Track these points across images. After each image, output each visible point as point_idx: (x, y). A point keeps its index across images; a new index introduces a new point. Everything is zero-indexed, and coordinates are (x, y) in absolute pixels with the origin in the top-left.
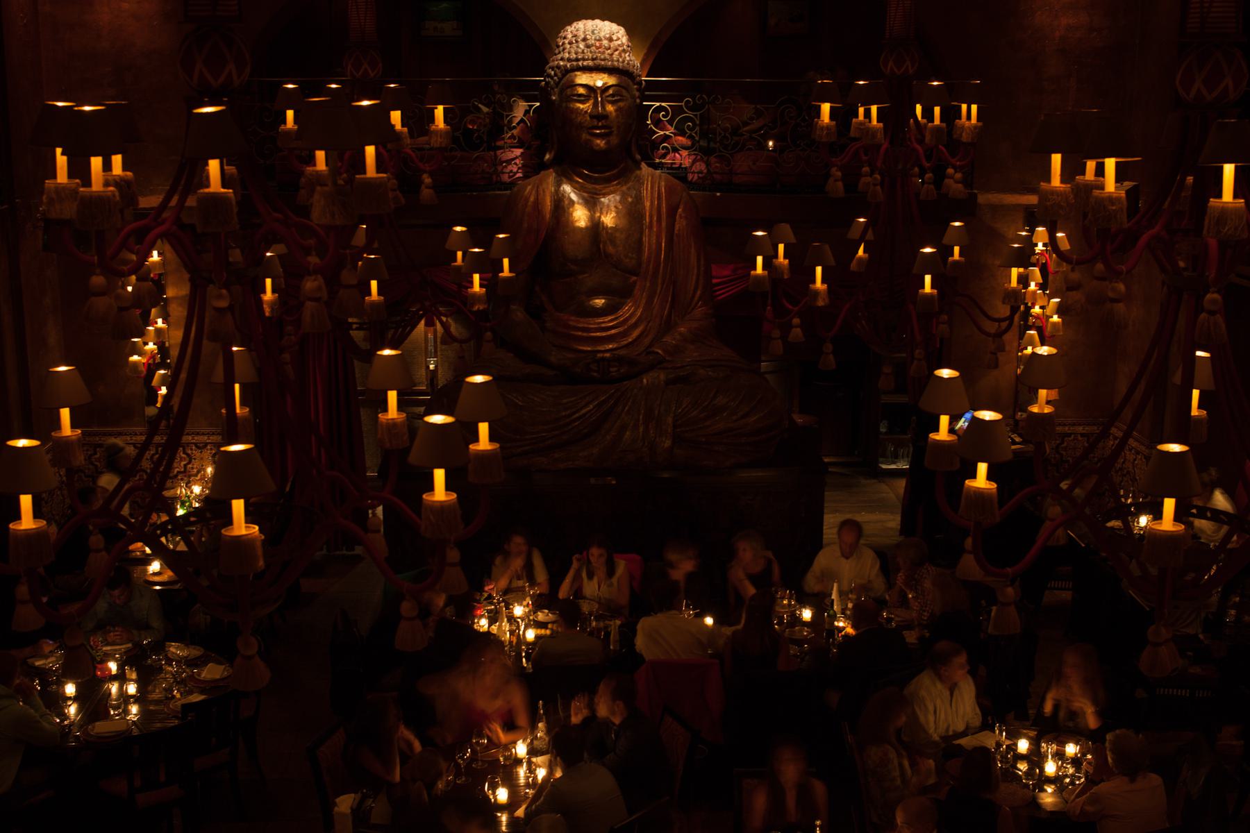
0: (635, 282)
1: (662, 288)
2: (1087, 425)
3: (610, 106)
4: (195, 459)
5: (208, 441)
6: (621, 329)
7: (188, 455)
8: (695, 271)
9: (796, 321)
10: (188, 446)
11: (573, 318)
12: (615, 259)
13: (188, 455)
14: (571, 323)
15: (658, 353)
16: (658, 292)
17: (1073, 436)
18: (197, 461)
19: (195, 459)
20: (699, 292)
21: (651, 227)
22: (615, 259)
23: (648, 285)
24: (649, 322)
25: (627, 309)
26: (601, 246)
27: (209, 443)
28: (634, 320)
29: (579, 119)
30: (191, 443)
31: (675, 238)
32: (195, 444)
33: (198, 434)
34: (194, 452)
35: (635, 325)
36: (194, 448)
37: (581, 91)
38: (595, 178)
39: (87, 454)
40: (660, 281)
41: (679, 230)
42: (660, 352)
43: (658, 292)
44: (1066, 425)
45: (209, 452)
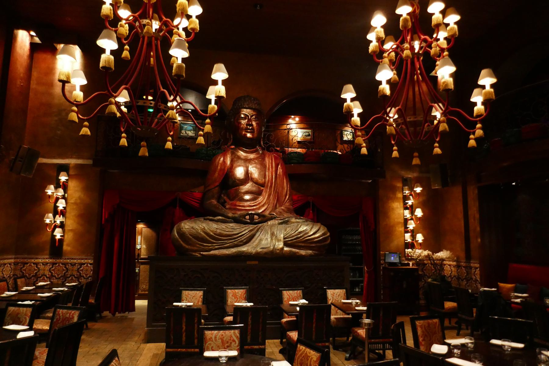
0: (263, 190)
1: (273, 193)
2: (43, 259)
3: (254, 122)
4: (69, 270)
5: (77, 262)
6: (258, 207)
7: (21, 272)
8: (286, 189)
9: (395, 148)
10: (67, 264)
11: (238, 202)
12: (255, 180)
13: (50, 272)
14: (237, 204)
15: (273, 214)
16: (272, 194)
17: (428, 265)
18: (45, 272)
19: (69, 270)
20: (287, 197)
21: (269, 169)
22: (255, 180)
23: (268, 190)
24: (269, 205)
25: (261, 199)
26: (250, 175)
27: (77, 263)
28: (262, 204)
29: (242, 126)
30: (69, 263)
31: (278, 175)
32: (71, 264)
33: (72, 259)
34: (70, 267)
35: (263, 206)
36: (70, 265)
37: (242, 116)
38: (247, 151)
39: (42, 266)
40: (273, 190)
41: (279, 173)
42: (275, 214)
43: (272, 194)
44: (40, 259)
45: (77, 267)
